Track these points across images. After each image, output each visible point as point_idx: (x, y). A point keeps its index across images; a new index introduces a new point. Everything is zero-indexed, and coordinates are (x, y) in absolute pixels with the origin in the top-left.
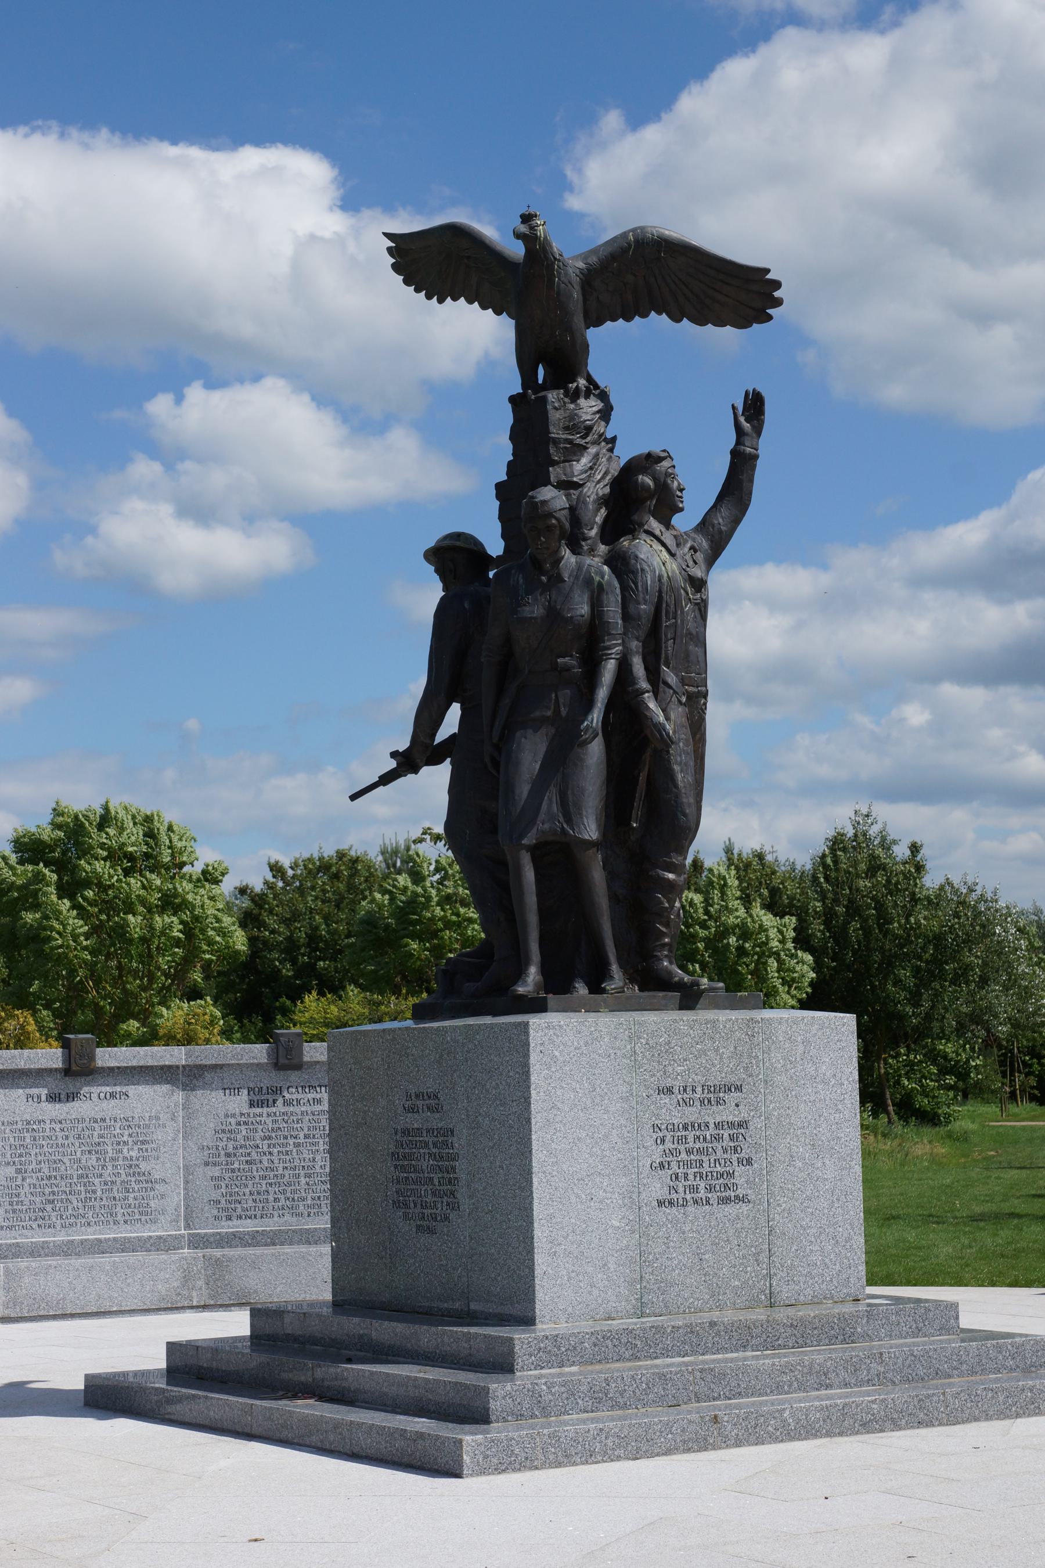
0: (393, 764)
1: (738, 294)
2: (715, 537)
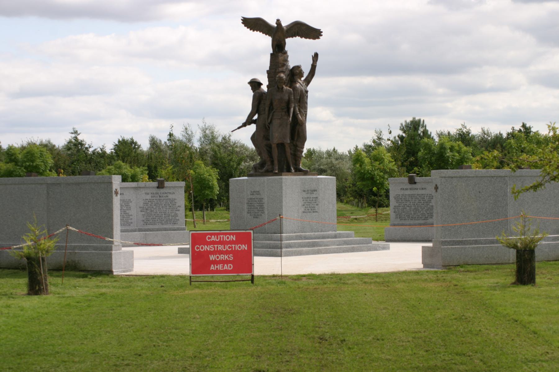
1: (312, 33)
2: (308, 81)
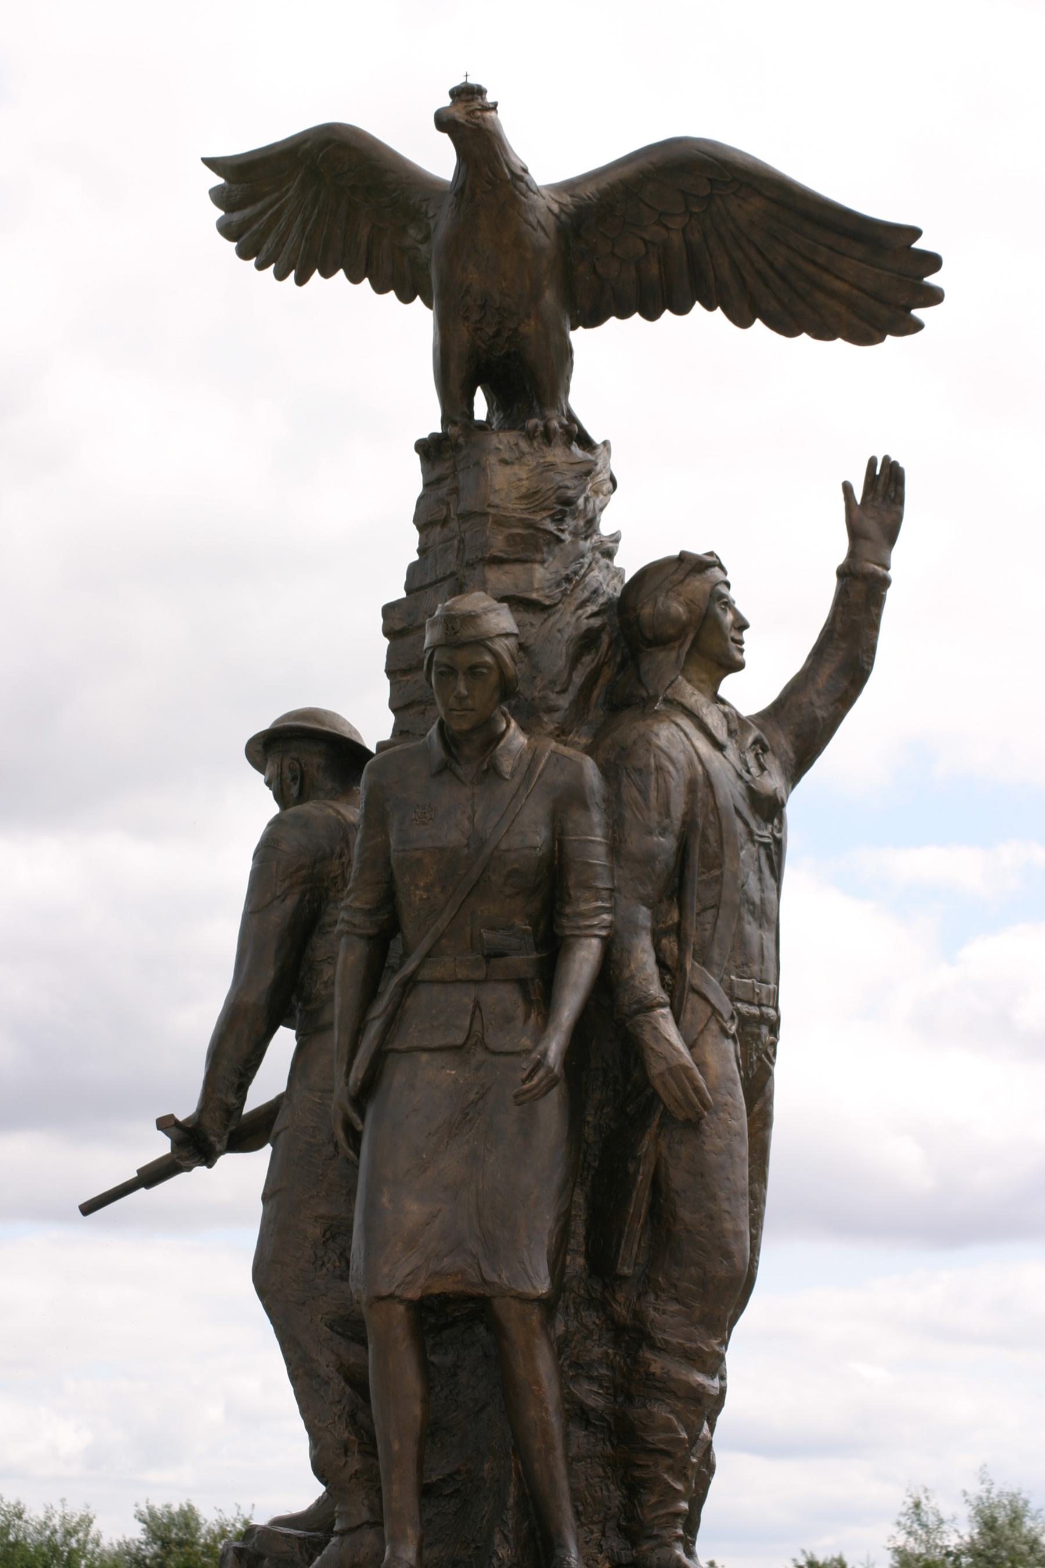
0: (161, 1146)
1: (846, 276)
